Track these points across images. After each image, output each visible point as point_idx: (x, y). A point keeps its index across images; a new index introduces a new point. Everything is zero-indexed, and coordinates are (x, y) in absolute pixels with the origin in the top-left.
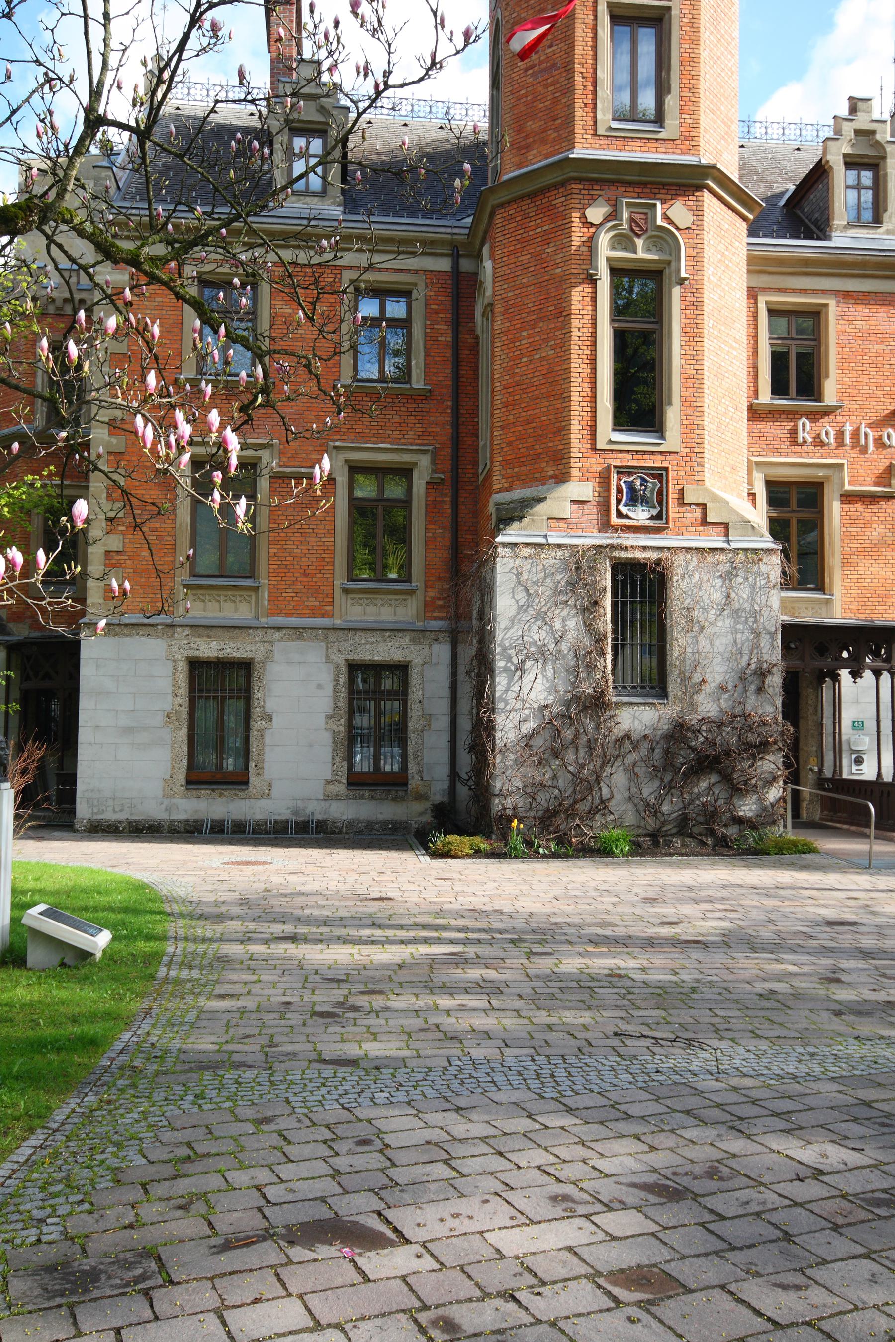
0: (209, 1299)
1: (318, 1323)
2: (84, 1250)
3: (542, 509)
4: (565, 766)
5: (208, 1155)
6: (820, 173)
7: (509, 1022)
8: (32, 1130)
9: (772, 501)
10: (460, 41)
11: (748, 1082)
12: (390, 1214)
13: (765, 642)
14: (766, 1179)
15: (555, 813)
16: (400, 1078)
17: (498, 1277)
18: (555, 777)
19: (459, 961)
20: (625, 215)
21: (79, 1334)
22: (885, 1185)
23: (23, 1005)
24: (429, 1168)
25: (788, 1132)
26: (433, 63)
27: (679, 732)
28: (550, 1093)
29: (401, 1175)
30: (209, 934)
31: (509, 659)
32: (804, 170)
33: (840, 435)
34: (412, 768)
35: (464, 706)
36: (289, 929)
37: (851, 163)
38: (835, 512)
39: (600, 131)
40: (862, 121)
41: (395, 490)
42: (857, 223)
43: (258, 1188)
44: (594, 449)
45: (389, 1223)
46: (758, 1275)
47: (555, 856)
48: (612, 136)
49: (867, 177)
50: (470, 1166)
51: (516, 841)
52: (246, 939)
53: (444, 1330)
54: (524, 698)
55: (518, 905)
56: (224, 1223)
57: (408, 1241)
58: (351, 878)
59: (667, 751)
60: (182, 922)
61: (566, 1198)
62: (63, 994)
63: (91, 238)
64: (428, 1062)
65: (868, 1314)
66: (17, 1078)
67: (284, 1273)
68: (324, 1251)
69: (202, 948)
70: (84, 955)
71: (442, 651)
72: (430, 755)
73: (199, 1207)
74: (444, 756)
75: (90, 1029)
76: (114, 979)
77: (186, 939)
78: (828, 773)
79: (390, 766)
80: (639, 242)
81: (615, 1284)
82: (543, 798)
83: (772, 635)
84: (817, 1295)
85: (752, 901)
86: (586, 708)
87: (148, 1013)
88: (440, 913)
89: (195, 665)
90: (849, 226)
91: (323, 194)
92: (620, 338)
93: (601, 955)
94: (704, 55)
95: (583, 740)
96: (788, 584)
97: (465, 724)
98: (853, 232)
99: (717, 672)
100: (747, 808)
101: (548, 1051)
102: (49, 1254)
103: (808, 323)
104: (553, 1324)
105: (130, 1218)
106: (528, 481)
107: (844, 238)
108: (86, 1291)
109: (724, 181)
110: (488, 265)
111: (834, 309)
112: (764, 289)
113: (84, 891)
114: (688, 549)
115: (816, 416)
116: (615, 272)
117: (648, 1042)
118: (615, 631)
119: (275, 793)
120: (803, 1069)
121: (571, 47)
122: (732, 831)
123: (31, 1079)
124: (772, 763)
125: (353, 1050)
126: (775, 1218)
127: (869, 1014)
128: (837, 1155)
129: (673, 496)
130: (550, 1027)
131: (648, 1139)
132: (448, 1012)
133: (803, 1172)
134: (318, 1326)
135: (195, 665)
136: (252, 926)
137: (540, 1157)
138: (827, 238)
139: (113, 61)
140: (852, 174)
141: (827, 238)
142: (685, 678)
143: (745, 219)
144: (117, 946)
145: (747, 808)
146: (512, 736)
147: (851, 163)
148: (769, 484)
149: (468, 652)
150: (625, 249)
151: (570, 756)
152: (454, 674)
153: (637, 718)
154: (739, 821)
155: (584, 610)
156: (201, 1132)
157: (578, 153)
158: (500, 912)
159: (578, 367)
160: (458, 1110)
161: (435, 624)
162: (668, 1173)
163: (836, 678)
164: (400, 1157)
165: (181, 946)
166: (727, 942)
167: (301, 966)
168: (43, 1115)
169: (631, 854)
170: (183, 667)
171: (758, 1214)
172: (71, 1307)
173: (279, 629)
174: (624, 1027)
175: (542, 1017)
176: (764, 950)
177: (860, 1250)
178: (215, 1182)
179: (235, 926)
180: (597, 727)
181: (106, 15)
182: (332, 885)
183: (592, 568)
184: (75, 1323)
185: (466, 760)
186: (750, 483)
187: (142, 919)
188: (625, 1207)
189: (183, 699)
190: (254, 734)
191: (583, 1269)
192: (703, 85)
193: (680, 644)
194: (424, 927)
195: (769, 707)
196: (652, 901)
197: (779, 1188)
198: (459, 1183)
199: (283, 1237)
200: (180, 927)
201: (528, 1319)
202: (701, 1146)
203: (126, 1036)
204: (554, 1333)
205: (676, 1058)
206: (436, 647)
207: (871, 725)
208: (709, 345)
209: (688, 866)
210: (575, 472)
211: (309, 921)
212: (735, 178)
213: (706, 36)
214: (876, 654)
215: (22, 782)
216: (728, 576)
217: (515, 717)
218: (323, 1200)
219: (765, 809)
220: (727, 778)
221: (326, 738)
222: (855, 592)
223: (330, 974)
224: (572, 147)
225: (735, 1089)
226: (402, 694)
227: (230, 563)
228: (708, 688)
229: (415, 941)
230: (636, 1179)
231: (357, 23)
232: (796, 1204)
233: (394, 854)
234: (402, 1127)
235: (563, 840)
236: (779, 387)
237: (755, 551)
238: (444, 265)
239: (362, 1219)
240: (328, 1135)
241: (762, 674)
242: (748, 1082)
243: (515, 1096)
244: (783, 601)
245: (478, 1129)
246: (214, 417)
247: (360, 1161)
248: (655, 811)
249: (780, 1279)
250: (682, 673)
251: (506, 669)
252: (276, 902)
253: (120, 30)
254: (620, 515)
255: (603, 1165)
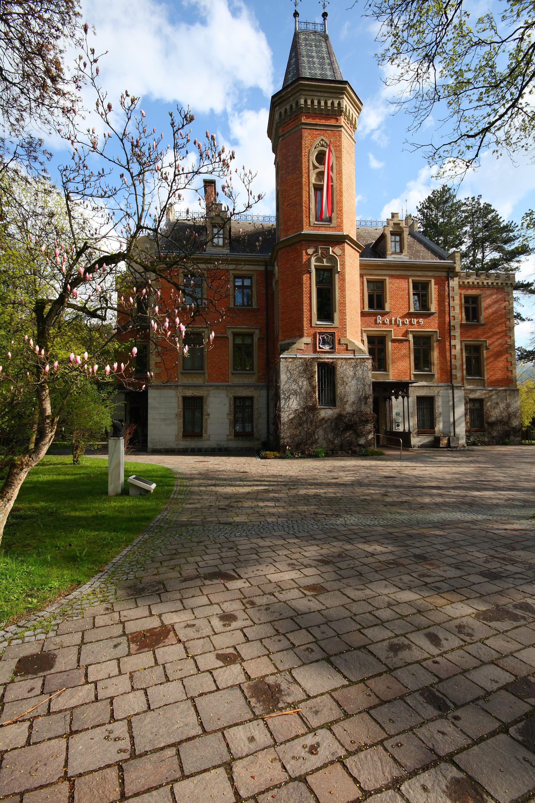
0: (178, 596)
1: (211, 603)
2: (141, 582)
3: (295, 346)
4: (303, 428)
5: (182, 553)
6: (383, 237)
7: (281, 510)
8: (127, 546)
9: (369, 342)
10: (256, 199)
11: (354, 527)
12: (237, 570)
13: (367, 388)
14: (356, 557)
15: (300, 444)
16: (244, 528)
17: (269, 588)
18: (300, 432)
19: (267, 491)
20: (320, 251)
21: (137, 607)
22: (393, 558)
23: (127, 507)
24: (250, 556)
25: (365, 542)
26: (249, 206)
27: (340, 417)
28: (291, 532)
29: (241, 558)
30: (188, 484)
31: (285, 395)
32: (378, 236)
33: (391, 321)
34: (255, 430)
35: (271, 410)
36: (213, 482)
37: (393, 234)
38: (390, 345)
39: (312, 225)
40: (396, 220)
41: (248, 341)
42: (395, 253)
43: (196, 563)
44: (311, 326)
45: (236, 572)
46: (350, 586)
47: (300, 458)
48: (315, 227)
49: (398, 238)
50: (264, 555)
51: (288, 453)
52: (200, 485)
53: (251, 604)
54: (290, 406)
55: (287, 473)
56: (184, 574)
57: (242, 578)
58: (235, 466)
59: (336, 423)
60: (179, 481)
61: (293, 564)
62: (140, 503)
63: (140, 264)
64: (254, 523)
65: (383, 597)
66: (123, 530)
67: (202, 588)
68: (215, 581)
69: (185, 489)
70: (148, 491)
71: (264, 393)
72: (261, 426)
73: (178, 569)
74: (265, 426)
75: (147, 515)
76: (157, 498)
77: (180, 486)
78: (388, 429)
79: (248, 429)
80: (325, 260)
81: (305, 590)
82: (296, 439)
83: (369, 386)
84: (368, 592)
85: (363, 470)
86: (310, 410)
87: (166, 509)
88: (262, 476)
89: (185, 398)
90: (392, 254)
91: (223, 246)
92: (319, 291)
93: (312, 489)
94: (344, 200)
95: (309, 420)
96: (374, 369)
97: (272, 416)
98: (393, 256)
99: (352, 398)
100: (362, 441)
101: (292, 519)
102: (131, 583)
103: (380, 285)
104: (285, 602)
105: (156, 572)
106: (290, 337)
107: (390, 258)
108: (140, 594)
109: (351, 240)
110: (276, 268)
111: (388, 280)
112: (366, 275)
113: (149, 471)
114: (342, 359)
115: (383, 315)
116: (317, 269)
117: (324, 516)
118: (319, 385)
119: (211, 439)
120: (372, 523)
121: (302, 198)
122: (357, 449)
123: (128, 530)
124: (370, 427)
125: (231, 520)
126: (358, 569)
127: (395, 505)
128: (379, 548)
129: (337, 342)
130: (293, 512)
131: (321, 546)
132: (262, 508)
133: (368, 555)
134: (211, 604)
135: (185, 398)
136: (201, 481)
137: (286, 552)
138: (386, 258)
139: (146, 208)
140: (393, 237)
141: (385, 257)
142: (341, 400)
143: (358, 252)
144: (158, 488)
145: (362, 441)
146: (286, 419)
147: (393, 234)
148: (368, 337)
149: (272, 392)
150: (320, 262)
151: (305, 426)
152: (268, 400)
153: (326, 413)
154: (360, 445)
155: (309, 379)
156: (180, 546)
157: (306, 231)
158: (281, 476)
159: (306, 300)
160: (262, 538)
161: (261, 384)
162: (326, 556)
163: (391, 399)
164: (242, 553)
165: (178, 488)
166: (353, 484)
167: (216, 494)
168: (131, 541)
169: (325, 456)
170: (180, 399)
171: (352, 568)
172: (135, 599)
173: (211, 386)
174: (317, 511)
175: (291, 509)
176: (364, 486)
177: (383, 578)
178: (183, 561)
179: (196, 482)
180: (314, 416)
181: (144, 194)
182: (228, 468)
183: (311, 365)
184: (136, 604)
185: (272, 427)
186: (362, 336)
187: (167, 480)
188: (311, 566)
189: (181, 410)
190: (204, 420)
191: (296, 586)
192: (344, 210)
193: (340, 389)
194: (257, 481)
195: (368, 409)
196: (330, 471)
197: (360, 560)
198: (260, 560)
199: (203, 577)
200: (179, 482)
201: (276, 601)
202: (336, 547)
203: (159, 516)
204: (285, 605)
205: (333, 521)
206: (262, 391)
207: (402, 414)
208: (347, 292)
209: (343, 460)
210: (305, 335)
211: (220, 479)
212: (355, 239)
213: (345, 194)
214: (403, 391)
215: (128, 437)
216: (355, 367)
217: (287, 413)
218: (216, 566)
219: (368, 441)
220: (355, 432)
221: (227, 421)
222: (396, 371)
223: (225, 496)
224: (302, 230)
225: (350, 530)
226: (251, 407)
227: (195, 364)
228: (349, 403)
229: (253, 485)
230: (315, 558)
231: (223, 194)
232: (365, 564)
233: (249, 458)
234: (244, 544)
235: (303, 453)
236: (371, 306)
237: (363, 359)
238: (262, 268)
239: (228, 572)
240: (220, 546)
241: (366, 398)
242: (354, 527)
243: (281, 533)
244: (372, 374)
245: (268, 543)
246: (177, 320)
247: (229, 554)
248: (333, 443)
249: (357, 587)
250: (340, 398)
251: (284, 398)
252: (210, 474)
253: (148, 199)
254: (320, 348)
255: (306, 554)
